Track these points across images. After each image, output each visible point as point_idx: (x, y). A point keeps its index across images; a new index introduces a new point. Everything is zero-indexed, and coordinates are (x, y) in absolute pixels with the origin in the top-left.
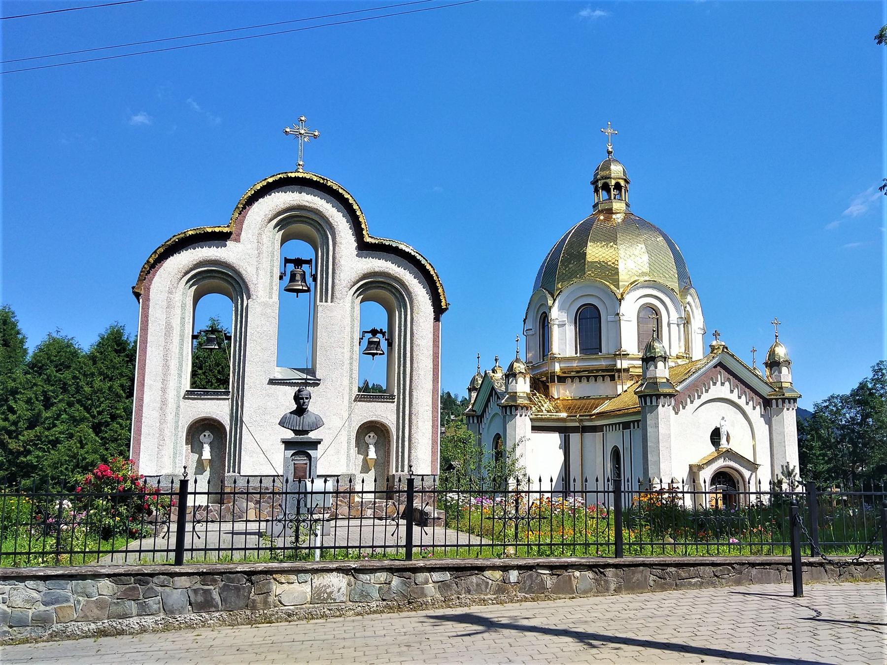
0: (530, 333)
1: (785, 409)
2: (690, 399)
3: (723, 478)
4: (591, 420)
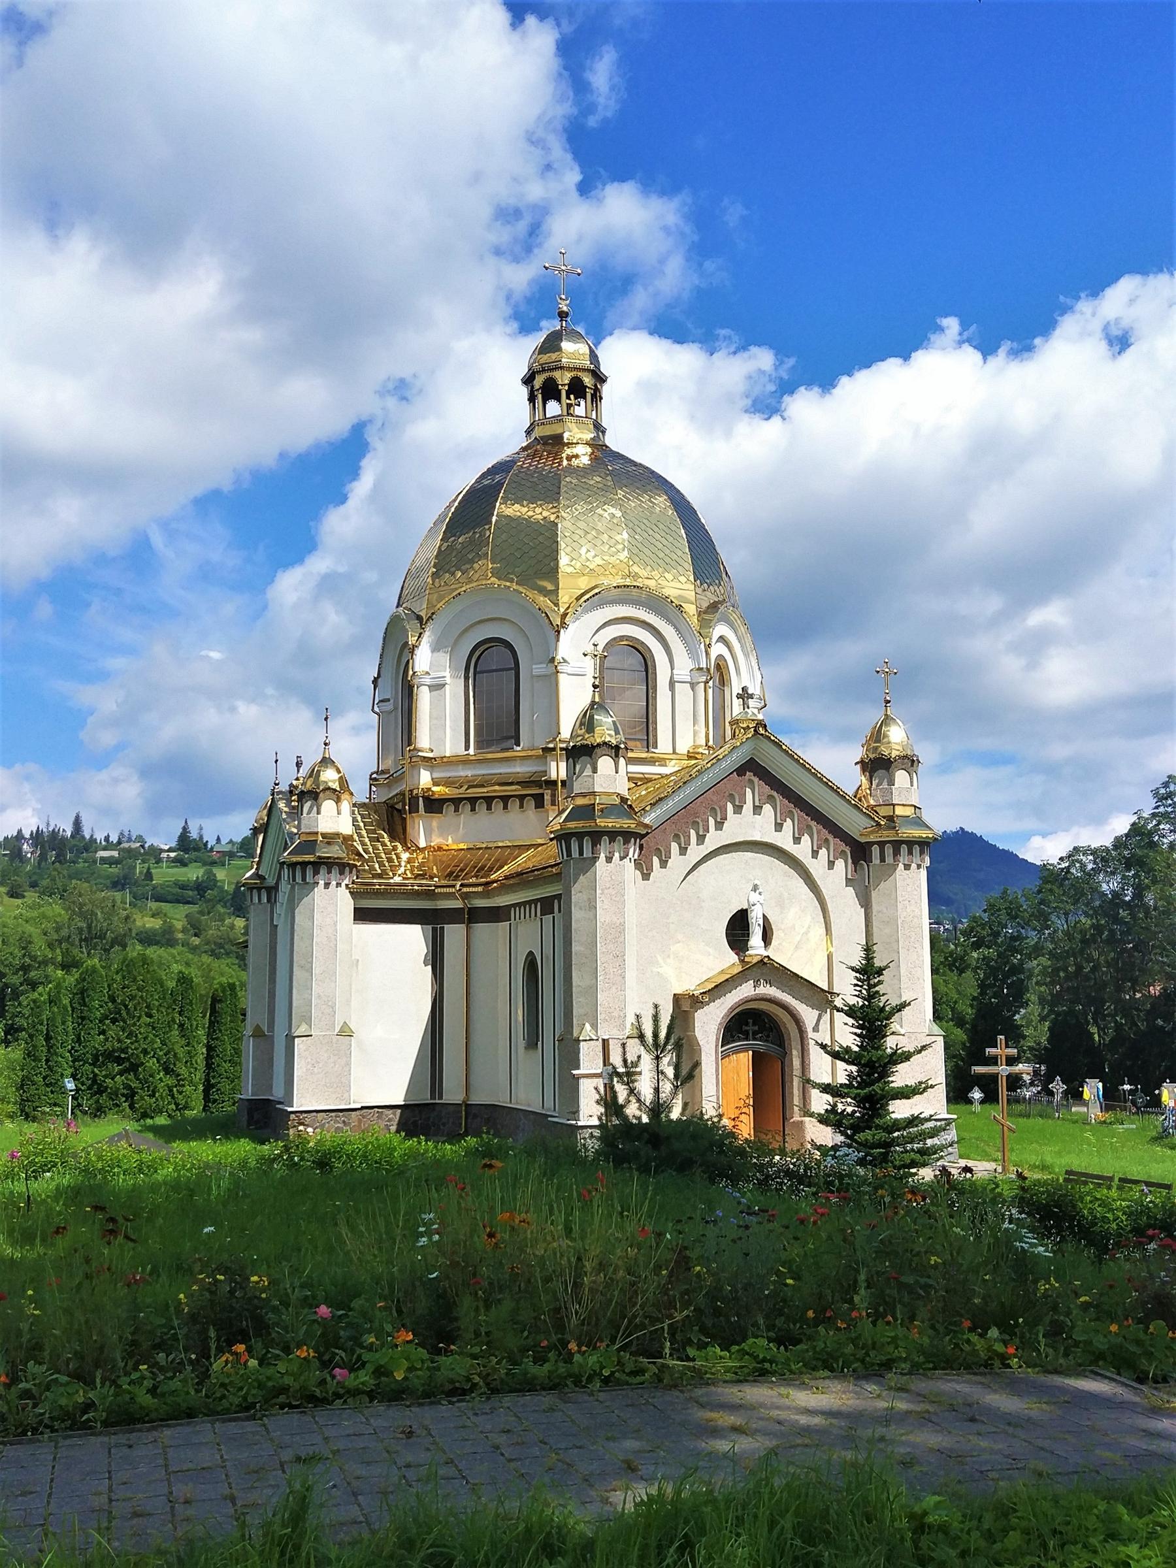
0: (388, 706)
1: (901, 866)
2: (680, 845)
3: (754, 1024)
4: (486, 894)
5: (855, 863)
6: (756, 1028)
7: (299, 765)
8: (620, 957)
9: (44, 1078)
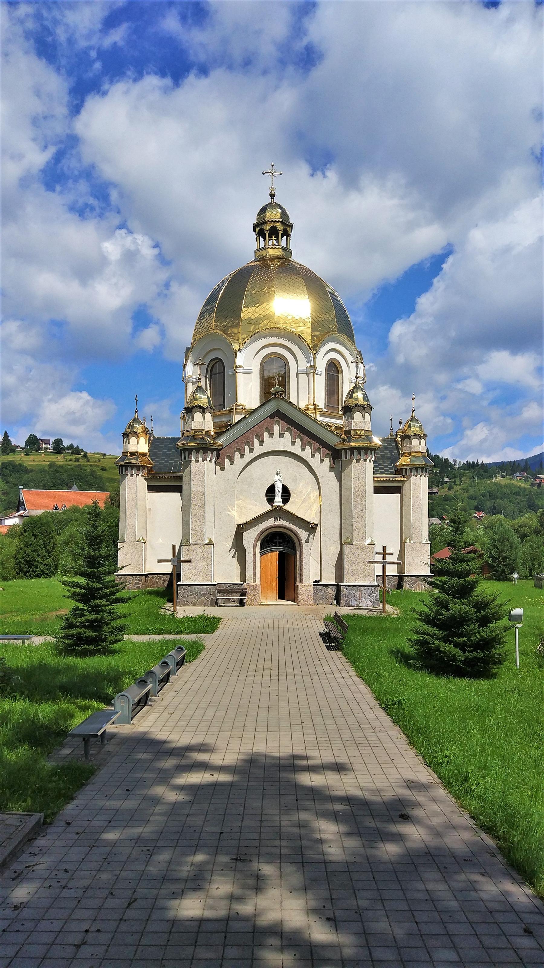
1: (355, 461)
3: (280, 539)
5: (334, 460)
6: (281, 541)
7: (400, 423)
8: (202, 507)
9: (113, 558)
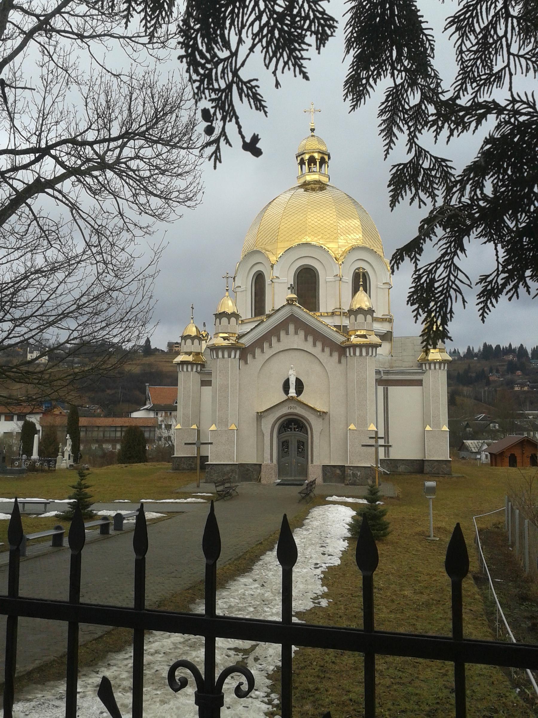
6: (296, 426)
